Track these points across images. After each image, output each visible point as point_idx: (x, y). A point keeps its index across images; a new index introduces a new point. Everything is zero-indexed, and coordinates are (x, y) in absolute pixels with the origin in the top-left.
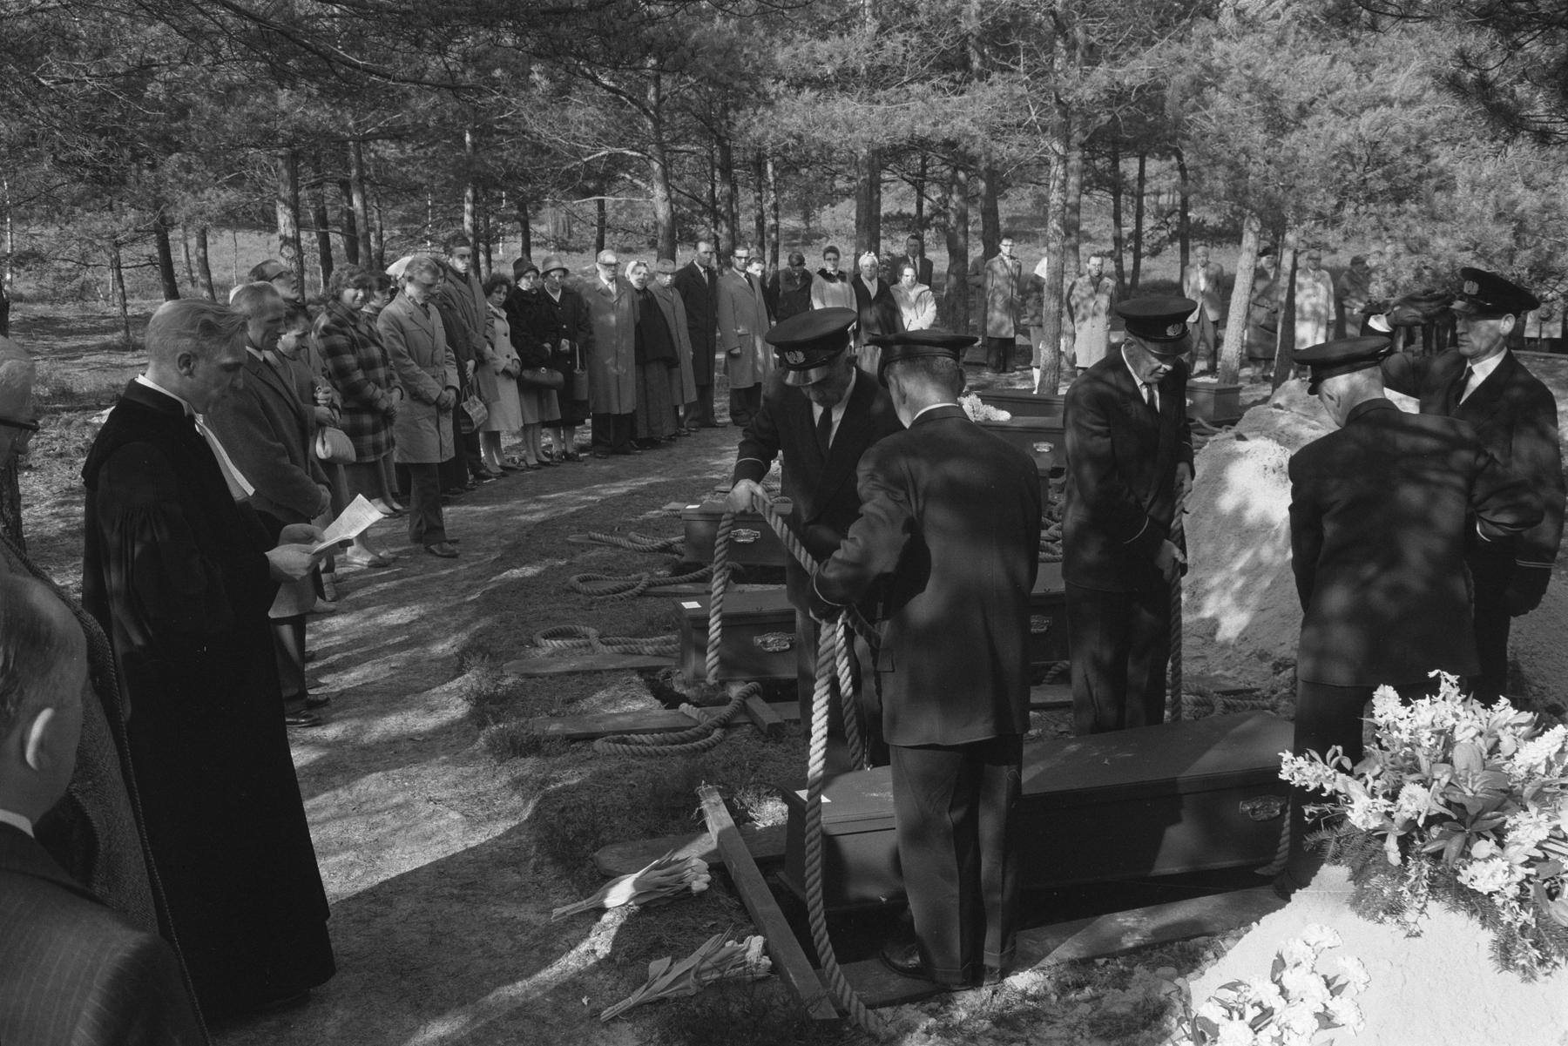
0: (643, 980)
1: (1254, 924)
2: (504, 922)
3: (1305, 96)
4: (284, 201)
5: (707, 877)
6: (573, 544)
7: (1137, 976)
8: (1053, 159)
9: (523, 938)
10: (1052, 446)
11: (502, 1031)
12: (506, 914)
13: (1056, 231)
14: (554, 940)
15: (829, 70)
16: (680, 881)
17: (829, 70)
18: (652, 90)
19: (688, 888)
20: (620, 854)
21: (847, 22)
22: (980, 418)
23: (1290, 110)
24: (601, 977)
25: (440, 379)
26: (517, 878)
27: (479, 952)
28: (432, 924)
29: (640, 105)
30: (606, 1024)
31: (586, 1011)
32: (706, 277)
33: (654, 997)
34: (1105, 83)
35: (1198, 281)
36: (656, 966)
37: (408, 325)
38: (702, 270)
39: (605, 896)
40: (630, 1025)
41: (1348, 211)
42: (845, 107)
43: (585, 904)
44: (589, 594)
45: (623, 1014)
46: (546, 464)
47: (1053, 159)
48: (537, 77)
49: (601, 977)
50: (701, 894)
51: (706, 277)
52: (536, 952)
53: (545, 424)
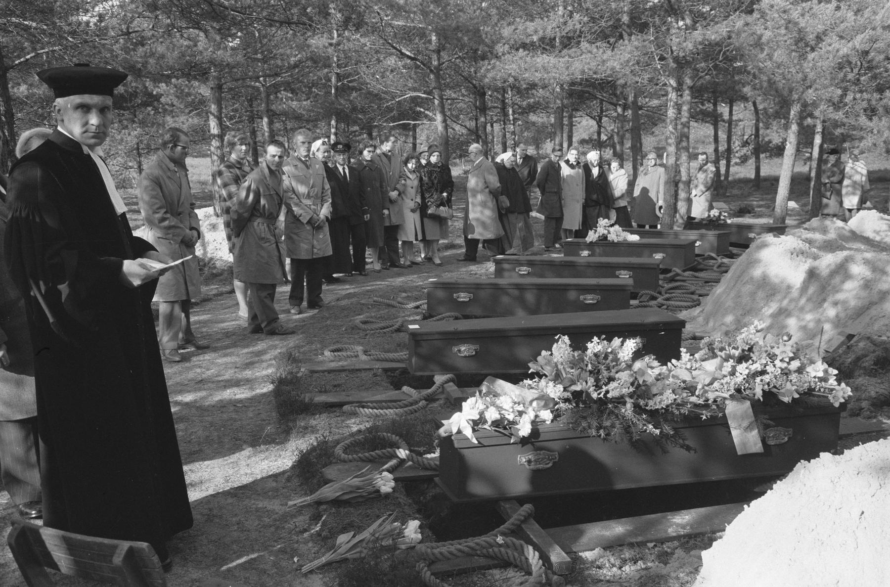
0: (333, 548)
1: (745, 506)
2: (257, 510)
3: (820, 28)
4: (213, 114)
5: (393, 484)
6: (363, 304)
7: (676, 556)
8: (670, 89)
9: (267, 520)
11: (235, 576)
12: (260, 506)
13: (671, 132)
14: (286, 522)
15: (535, 38)
16: (370, 484)
17: (535, 38)
19: (378, 491)
20: (339, 470)
21: (547, 11)
22: (621, 239)
23: (811, 37)
24: (310, 544)
26: (274, 484)
27: (236, 528)
28: (210, 510)
29: (429, 68)
30: (305, 575)
31: (295, 566)
33: (338, 558)
34: (701, 40)
36: (342, 538)
40: (321, 576)
41: (849, 97)
42: (542, 59)
44: (365, 330)
45: (318, 568)
47: (670, 89)
48: (333, 11)
49: (310, 544)
50: (387, 496)
52: (273, 529)
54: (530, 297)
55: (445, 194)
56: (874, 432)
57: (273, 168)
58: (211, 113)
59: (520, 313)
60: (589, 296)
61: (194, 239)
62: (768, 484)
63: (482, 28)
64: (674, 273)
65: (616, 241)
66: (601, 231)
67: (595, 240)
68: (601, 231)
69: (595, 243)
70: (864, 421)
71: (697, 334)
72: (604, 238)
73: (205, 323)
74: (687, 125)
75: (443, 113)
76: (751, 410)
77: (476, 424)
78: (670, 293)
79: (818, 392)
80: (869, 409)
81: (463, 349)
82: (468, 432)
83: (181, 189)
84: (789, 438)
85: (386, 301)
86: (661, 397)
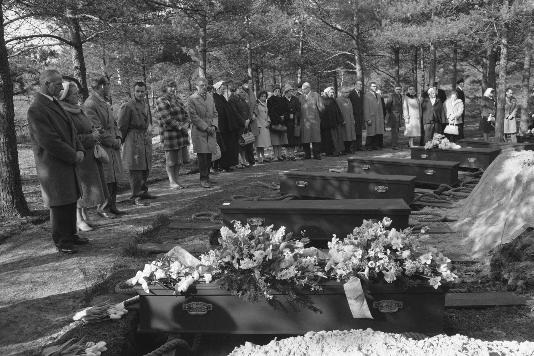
4: (201, 67)
8: (502, 46)
10: (475, 159)
15: (408, 15)
17: (408, 15)
18: (356, 29)
22: (447, 148)
25: (209, 123)
32: (359, 94)
35: (268, 28)
37: (196, 102)
38: (357, 92)
39: (74, 315)
42: (412, 28)
43: (66, 317)
46: (282, 160)
51: (359, 94)
53: (284, 146)
54: (346, 187)
55: (282, 117)
56: (515, 305)
57: (139, 98)
58: (199, 66)
59: (339, 197)
60: (381, 187)
61: (120, 144)
62: (424, 336)
63: (375, 9)
64: (480, 172)
65: (443, 149)
66: (435, 141)
67: (430, 148)
68: (435, 141)
69: (430, 149)
70: (516, 295)
71: (448, 218)
72: (436, 146)
73: (153, 192)
74: (529, 70)
75: (361, 64)
76: (361, 285)
77: (150, 279)
78: (466, 186)
79: (426, 275)
80: (521, 287)
81: (254, 220)
82: (145, 286)
83: (108, 113)
84: (399, 309)
85: (263, 183)
86: (286, 271)
